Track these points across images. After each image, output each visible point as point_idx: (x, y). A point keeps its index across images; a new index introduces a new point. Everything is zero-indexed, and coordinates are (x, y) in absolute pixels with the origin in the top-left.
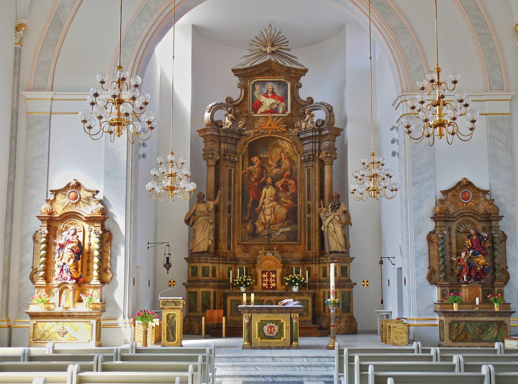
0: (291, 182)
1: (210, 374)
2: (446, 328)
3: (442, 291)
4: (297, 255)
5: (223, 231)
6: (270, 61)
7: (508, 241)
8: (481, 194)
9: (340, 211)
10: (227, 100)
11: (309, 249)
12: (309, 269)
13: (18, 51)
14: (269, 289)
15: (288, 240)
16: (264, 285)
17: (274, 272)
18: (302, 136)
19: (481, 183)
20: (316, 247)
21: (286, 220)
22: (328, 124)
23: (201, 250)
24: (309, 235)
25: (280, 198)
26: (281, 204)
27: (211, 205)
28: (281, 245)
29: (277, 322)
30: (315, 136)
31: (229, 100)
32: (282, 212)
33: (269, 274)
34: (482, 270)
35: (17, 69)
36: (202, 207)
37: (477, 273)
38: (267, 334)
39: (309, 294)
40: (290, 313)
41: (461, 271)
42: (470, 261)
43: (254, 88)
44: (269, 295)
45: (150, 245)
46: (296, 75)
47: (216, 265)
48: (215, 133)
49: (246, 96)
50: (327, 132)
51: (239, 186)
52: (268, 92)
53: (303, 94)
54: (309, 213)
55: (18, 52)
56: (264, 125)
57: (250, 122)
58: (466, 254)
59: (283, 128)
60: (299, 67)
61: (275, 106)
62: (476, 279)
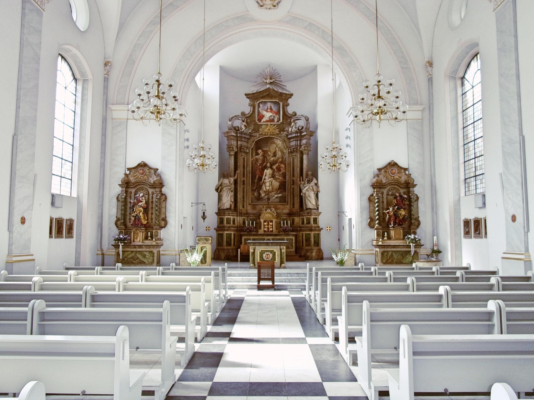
0: (282, 165)
1: (442, 290)
2: (380, 255)
3: (377, 232)
4: (286, 211)
5: (239, 196)
6: (269, 88)
7: (420, 200)
8: (403, 171)
9: (312, 184)
10: (242, 114)
11: (293, 207)
12: (293, 220)
13: (106, 79)
14: (268, 231)
15: (280, 202)
16: (265, 229)
17: (272, 221)
18: (289, 136)
19: (403, 163)
20: (297, 206)
21: (279, 189)
22: (306, 128)
23: (225, 208)
24: (293, 199)
25: (275, 176)
26: (276, 179)
27: (232, 180)
28: (276, 205)
29: (271, 252)
30: (298, 136)
31: (243, 114)
32: (276, 184)
33: (268, 223)
34: (403, 218)
35: (106, 91)
36: (226, 181)
37: (400, 221)
38: (265, 259)
39: (293, 235)
40: (280, 245)
41: (389, 219)
42: (395, 213)
43: (259, 106)
44: (268, 235)
45: (193, 204)
46: (285, 97)
47: (236, 217)
48: (234, 135)
49: (254, 111)
50: (305, 133)
51: (249, 169)
52: (268, 109)
53: (290, 110)
54: (293, 185)
55: (106, 80)
56: (267, 130)
57: (257, 128)
58: (393, 209)
59: (277, 131)
60: (287, 93)
61: (272, 117)
62: (399, 225)
